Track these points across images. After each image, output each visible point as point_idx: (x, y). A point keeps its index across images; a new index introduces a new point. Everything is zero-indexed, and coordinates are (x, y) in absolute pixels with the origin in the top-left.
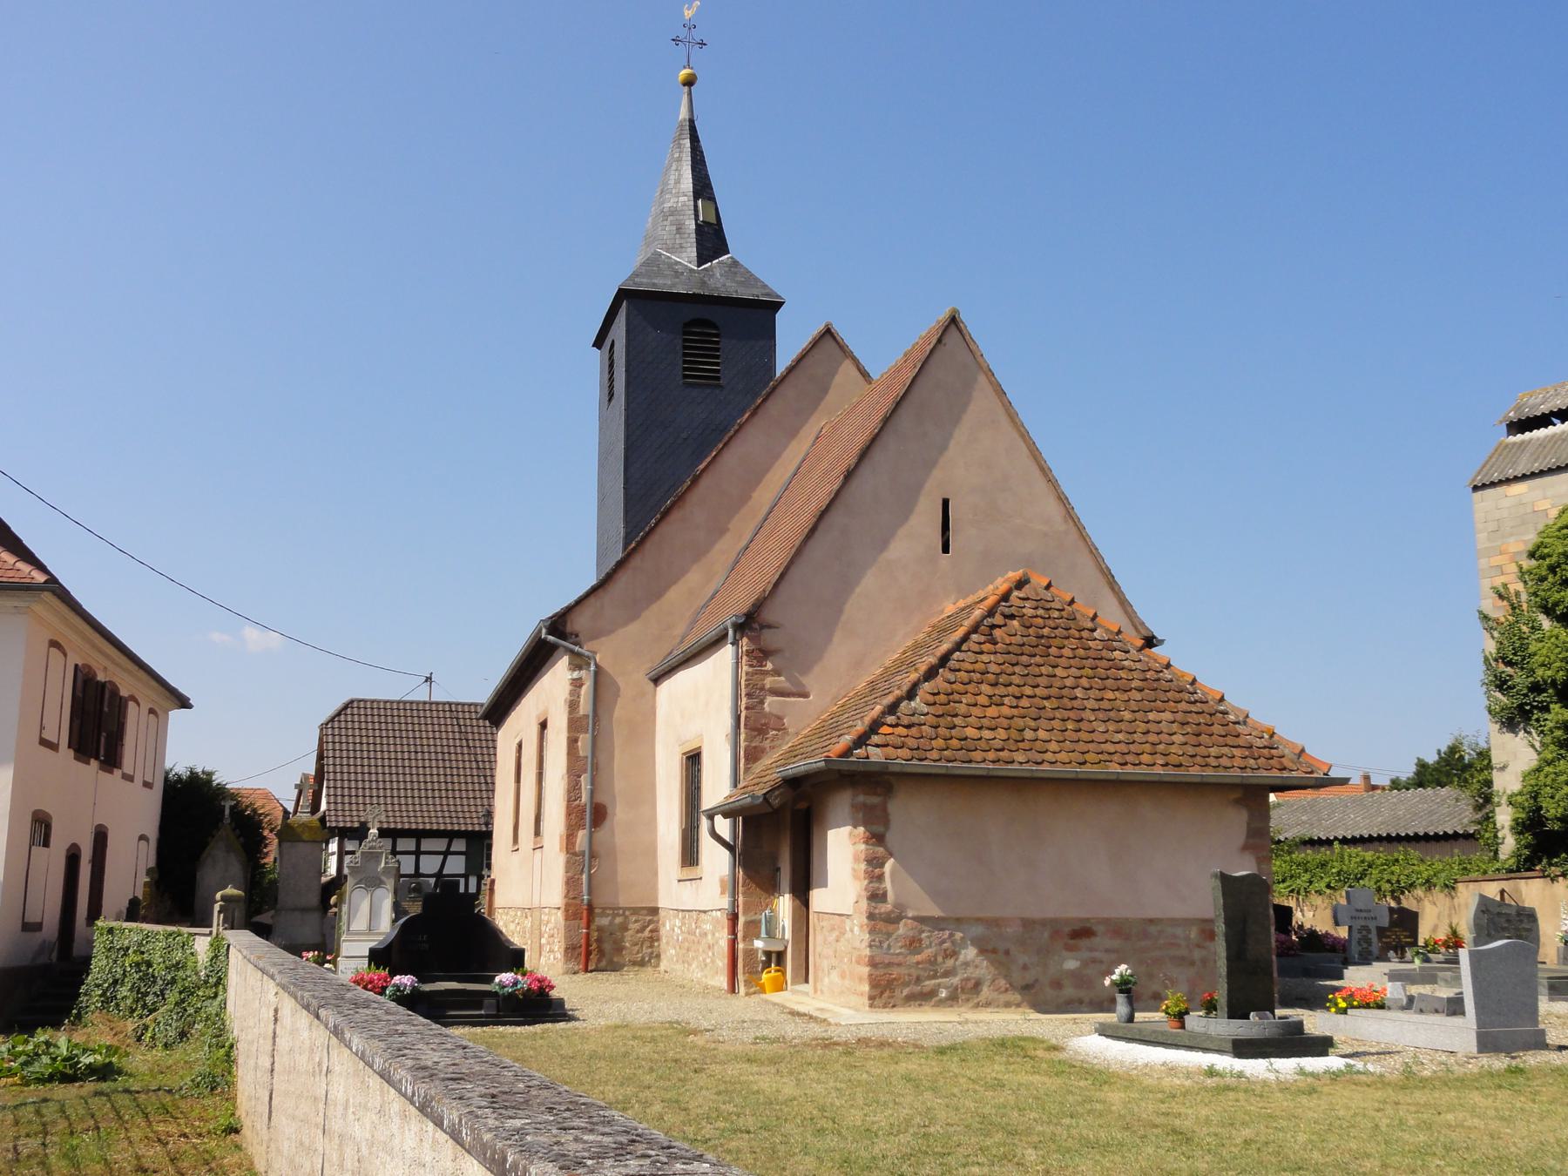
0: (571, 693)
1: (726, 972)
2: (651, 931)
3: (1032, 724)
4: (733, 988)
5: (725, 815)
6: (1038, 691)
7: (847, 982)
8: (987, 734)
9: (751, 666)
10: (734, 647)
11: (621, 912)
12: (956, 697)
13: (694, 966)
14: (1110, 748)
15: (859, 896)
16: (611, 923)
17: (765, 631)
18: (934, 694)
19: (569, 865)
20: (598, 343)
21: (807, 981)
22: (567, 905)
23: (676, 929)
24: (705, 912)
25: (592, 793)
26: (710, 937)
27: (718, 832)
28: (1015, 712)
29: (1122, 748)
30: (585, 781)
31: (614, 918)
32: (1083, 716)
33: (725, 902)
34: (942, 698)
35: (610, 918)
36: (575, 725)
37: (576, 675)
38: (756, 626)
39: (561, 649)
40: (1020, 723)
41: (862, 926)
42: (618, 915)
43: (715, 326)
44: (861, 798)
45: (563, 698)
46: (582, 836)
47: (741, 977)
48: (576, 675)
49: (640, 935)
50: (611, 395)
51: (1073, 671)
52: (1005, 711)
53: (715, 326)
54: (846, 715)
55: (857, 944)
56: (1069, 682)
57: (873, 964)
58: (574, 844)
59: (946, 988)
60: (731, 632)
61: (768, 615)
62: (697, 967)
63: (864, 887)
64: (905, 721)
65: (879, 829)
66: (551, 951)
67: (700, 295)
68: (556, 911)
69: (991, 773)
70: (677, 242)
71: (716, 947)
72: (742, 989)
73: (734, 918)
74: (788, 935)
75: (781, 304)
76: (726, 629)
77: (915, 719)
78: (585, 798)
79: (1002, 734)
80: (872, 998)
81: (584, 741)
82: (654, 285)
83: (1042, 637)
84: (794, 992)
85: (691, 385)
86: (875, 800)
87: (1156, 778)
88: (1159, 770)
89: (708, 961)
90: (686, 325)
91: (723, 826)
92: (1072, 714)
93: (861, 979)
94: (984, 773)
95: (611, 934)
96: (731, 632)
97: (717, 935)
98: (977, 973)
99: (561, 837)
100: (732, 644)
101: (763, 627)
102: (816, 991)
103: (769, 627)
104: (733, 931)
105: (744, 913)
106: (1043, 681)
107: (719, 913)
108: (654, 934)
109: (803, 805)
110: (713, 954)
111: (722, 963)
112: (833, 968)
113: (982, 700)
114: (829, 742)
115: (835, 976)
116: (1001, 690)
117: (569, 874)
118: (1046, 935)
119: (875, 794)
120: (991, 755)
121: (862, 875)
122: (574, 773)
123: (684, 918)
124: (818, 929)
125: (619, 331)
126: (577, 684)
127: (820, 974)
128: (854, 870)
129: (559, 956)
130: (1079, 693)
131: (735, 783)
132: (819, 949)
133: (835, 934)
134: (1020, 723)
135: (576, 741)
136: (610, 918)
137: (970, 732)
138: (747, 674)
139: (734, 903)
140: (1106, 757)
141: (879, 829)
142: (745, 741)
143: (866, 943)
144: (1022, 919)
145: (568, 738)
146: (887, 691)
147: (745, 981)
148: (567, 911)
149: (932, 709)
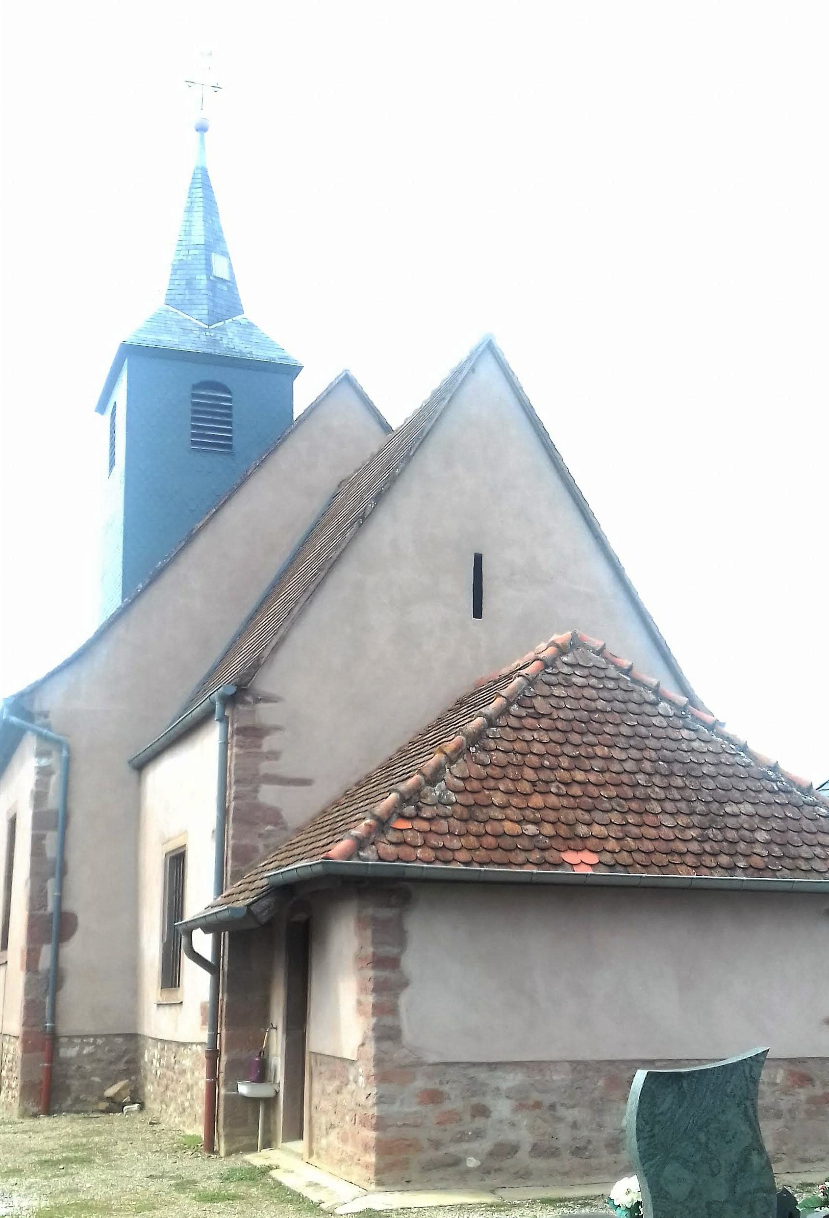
0: (38, 783)
1: (203, 1120)
2: (127, 1062)
3: (587, 817)
4: (210, 1147)
5: (206, 929)
6: (592, 778)
7: (349, 1149)
8: (531, 829)
9: (241, 747)
10: (223, 725)
11: (92, 1040)
12: (492, 783)
13: (171, 1109)
14: (681, 847)
15: (365, 1038)
16: (79, 1054)
17: (261, 706)
18: (463, 779)
19: (29, 987)
20: (101, 408)
21: (301, 1137)
22: (26, 1034)
23: (154, 1061)
24: (184, 1045)
25: (60, 900)
26: (189, 1075)
27: (196, 950)
28: (565, 802)
29: (694, 847)
30: (51, 885)
31: (82, 1049)
32: (647, 807)
33: (204, 1036)
34: (475, 785)
35: (77, 1048)
36: (40, 822)
37: (44, 762)
38: (249, 699)
39: (29, 733)
40: (571, 815)
41: (368, 1078)
42: (88, 1044)
43: (226, 390)
44: (370, 911)
45: (30, 790)
46: (46, 952)
47: (221, 1130)
48: (44, 762)
49: (113, 1067)
50: (112, 463)
51: (634, 753)
52: (553, 800)
53: (226, 390)
54: (355, 807)
55: (362, 1099)
56: (629, 766)
57: (380, 1125)
58: (36, 961)
59: (476, 1156)
60: (218, 706)
61: (265, 683)
62: (175, 1110)
63: (371, 1026)
64: (427, 813)
65: (390, 951)
66: (9, 1087)
67: (210, 355)
68: (13, 1040)
69: (534, 878)
70: (187, 298)
71: (195, 1089)
72: (222, 1146)
73: (213, 1055)
74: (281, 1078)
75: (300, 368)
76: (213, 704)
77: (441, 810)
78: (51, 907)
79: (548, 829)
80: (378, 1172)
81: (51, 840)
82: (159, 341)
83: (597, 710)
84: (283, 1150)
85: (198, 450)
86: (386, 913)
87: (686, 884)
88: (740, 876)
89: (187, 1104)
90: (195, 387)
91: (203, 943)
92: (634, 805)
93: (366, 1147)
94: (637, 882)
95: (79, 1067)
96: (218, 706)
97: (197, 1074)
98: (511, 1136)
99: (22, 952)
100: (220, 720)
101: (257, 701)
102: (311, 1153)
103: (268, 699)
104: (212, 1071)
105: (227, 1051)
106: (597, 764)
107: (199, 1047)
108: (131, 1066)
109: (300, 917)
110: (192, 1096)
111: (200, 1109)
112: (332, 1126)
113: (525, 787)
114: (330, 839)
115: (333, 1136)
116: (545, 775)
117: (30, 997)
118: (601, 1083)
119: (389, 906)
120: (536, 856)
121: (369, 1009)
122: (38, 875)
123: (163, 1049)
124: (315, 1074)
125: (120, 395)
126: (44, 773)
127: (316, 1132)
128: (359, 1003)
129: (17, 1094)
130: (641, 779)
131: (220, 888)
132: (315, 1100)
133: (337, 1083)
134: (571, 815)
135: (43, 837)
136: (77, 1048)
137: (509, 826)
138: (237, 756)
139: (214, 1038)
140: (677, 859)
141: (390, 951)
142: (233, 838)
143: (372, 1100)
144: (571, 1062)
145: (33, 836)
146: (405, 776)
147: (226, 1136)
148: (25, 1042)
149: (461, 798)
